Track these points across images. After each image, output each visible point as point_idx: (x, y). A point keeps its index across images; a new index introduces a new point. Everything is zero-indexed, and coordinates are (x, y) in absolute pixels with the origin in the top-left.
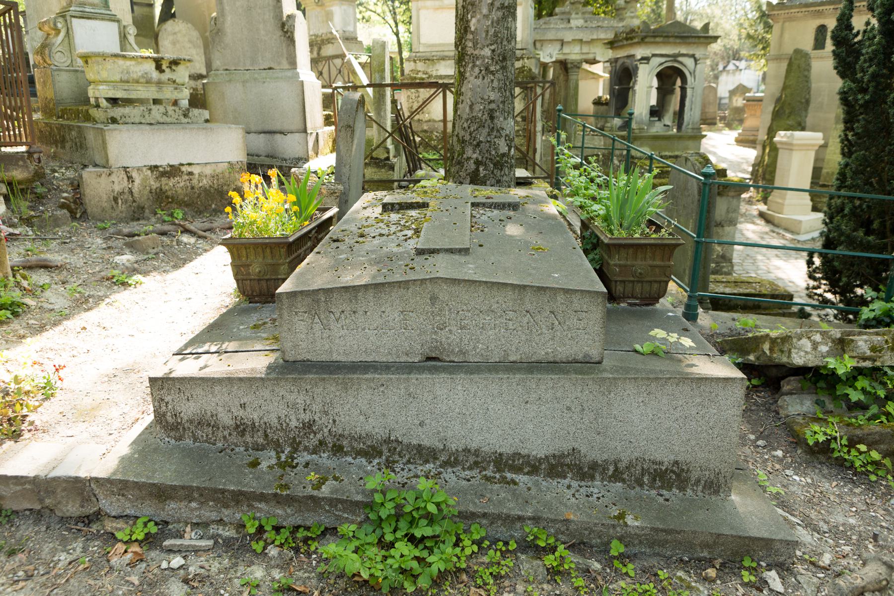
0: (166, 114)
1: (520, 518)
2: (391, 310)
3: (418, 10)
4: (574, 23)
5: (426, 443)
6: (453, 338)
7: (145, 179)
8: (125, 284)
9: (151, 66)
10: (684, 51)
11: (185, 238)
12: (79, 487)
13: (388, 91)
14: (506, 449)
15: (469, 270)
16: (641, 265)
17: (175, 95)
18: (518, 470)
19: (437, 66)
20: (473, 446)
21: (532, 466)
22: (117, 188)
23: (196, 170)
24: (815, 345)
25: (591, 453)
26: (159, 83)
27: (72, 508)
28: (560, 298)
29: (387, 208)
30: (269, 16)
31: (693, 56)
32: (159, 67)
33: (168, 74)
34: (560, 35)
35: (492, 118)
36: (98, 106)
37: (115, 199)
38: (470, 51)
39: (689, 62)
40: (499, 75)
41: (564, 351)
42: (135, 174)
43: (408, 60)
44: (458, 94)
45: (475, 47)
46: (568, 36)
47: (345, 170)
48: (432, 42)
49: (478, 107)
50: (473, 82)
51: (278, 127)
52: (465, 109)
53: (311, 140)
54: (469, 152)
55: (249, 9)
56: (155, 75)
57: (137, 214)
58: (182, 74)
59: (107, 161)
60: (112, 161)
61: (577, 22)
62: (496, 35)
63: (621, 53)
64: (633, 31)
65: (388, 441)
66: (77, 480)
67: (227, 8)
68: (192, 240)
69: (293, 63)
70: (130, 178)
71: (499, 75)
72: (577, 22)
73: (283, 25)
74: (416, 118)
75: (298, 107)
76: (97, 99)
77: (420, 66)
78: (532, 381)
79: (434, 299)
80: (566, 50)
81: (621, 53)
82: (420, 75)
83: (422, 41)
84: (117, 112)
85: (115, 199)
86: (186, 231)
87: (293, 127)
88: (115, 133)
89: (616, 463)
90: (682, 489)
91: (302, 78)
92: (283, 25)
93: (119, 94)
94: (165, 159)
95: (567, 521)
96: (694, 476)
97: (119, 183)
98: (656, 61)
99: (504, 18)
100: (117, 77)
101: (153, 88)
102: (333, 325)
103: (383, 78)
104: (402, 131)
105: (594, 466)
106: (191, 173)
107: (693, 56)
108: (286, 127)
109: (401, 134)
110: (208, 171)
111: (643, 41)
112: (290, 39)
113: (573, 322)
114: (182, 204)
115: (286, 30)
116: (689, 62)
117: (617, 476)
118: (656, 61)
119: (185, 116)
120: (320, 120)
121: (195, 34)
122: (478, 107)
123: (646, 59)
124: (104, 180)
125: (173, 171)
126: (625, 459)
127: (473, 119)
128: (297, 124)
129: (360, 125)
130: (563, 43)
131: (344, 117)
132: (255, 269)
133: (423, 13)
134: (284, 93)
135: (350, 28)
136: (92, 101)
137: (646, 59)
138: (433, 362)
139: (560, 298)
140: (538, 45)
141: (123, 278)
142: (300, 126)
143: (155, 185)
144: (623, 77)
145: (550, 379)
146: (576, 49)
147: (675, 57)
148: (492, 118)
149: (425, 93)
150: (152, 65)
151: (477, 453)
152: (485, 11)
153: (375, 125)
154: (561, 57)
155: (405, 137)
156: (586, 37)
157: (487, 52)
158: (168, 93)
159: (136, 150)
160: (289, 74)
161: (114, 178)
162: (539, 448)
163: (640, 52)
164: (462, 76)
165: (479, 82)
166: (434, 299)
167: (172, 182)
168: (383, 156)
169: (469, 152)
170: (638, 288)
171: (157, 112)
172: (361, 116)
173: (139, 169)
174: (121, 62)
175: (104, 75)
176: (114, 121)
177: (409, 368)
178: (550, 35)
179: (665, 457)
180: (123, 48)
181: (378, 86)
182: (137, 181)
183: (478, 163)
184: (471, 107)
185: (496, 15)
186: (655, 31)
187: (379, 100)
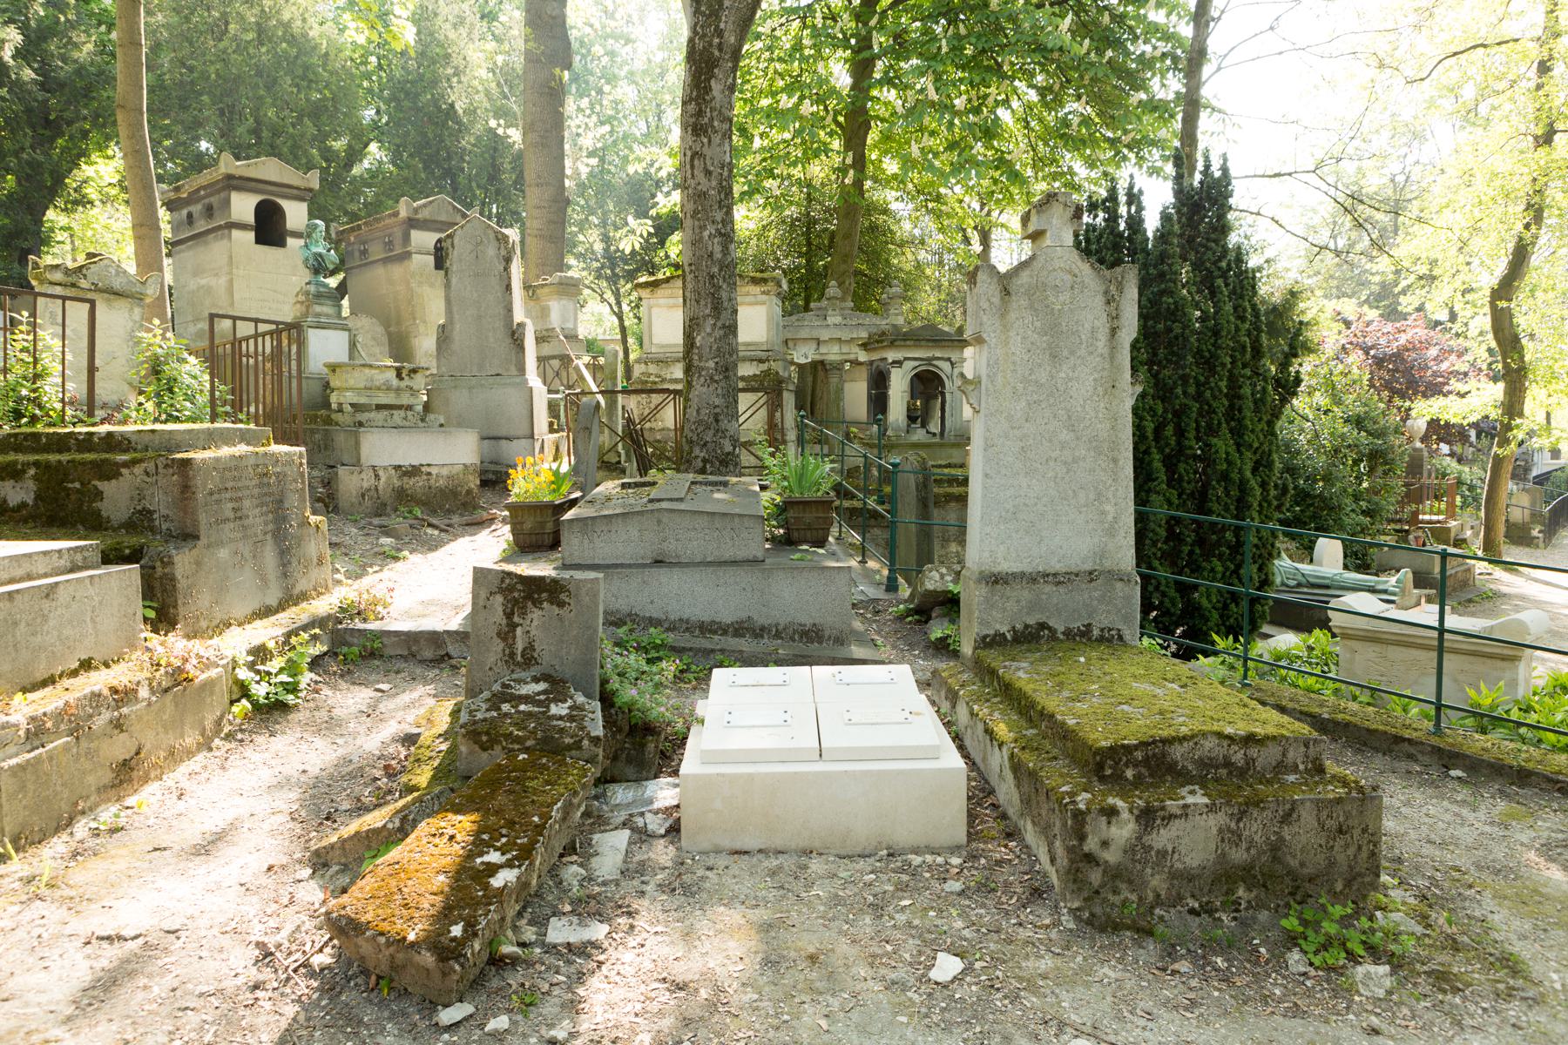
0: (405, 419)
1: (713, 651)
2: (632, 530)
3: (650, 308)
4: (830, 320)
5: (655, 615)
6: (671, 547)
7: (389, 478)
8: (396, 559)
9: (392, 374)
10: (938, 355)
11: (429, 531)
12: (435, 638)
13: (620, 397)
14: (706, 618)
15: (682, 506)
16: (809, 516)
17: (411, 401)
18: (715, 632)
19: (672, 369)
20: (685, 617)
21: (723, 630)
22: (365, 485)
23: (434, 471)
24: (942, 576)
25: (761, 620)
26: (398, 389)
27: (428, 654)
28: (737, 520)
29: (624, 486)
30: (499, 324)
31: (949, 359)
32: (399, 376)
33: (407, 382)
34: (815, 334)
35: (717, 421)
36: (340, 410)
37: (363, 495)
38: (696, 363)
39: (945, 366)
40: (722, 384)
41: (742, 554)
42: (381, 473)
43: (638, 361)
44: (687, 400)
45: (700, 359)
46: (825, 335)
47: (582, 467)
48: (665, 342)
49: (705, 411)
50: (699, 389)
51: (503, 433)
52: (692, 413)
53: (538, 446)
54: (697, 451)
55: (480, 317)
56: (395, 382)
57: (380, 510)
58: (419, 381)
59: (359, 460)
60: (363, 461)
61: (835, 319)
62: (718, 349)
63: (875, 356)
64: (883, 333)
65: (630, 615)
66: (435, 633)
67: (456, 316)
68: (436, 532)
69: (522, 370)
70: (377, 476)
71: (722, 384)
72: (835, 319)
73: (513, 333)
74: (648, 425)
75: (525, 412)
76: (340, 404)
77: (652, 368)
78: (720, 571)
79: (659, 522)
80: (823, 350)
81: (875, 356)
82: (652, 378)
83: (655, 341)
84: (363, 417)
85: (363, 495)
86: (430, 525)
87: (520, 433)
88: (369, 436)
89: (777, 625)
90: (820, 643)
91: (531, 384)
92: (513, 333)
93: (363, 400)
94: (409, 458)
95: (741, 652)
96: (827, 633)
97: (367, 480)
98: (909, 365)
99: (726, 335)
100: (362, 385)
101: (392, 395)
102: (596, 540)
103: (615, 385)
104: (634, 436)
105: (763, 629)
106: (429, 474)
107: (949, 359)
108: (512, 433)
109: (632, 439)
110: (445, 471)
111: (892, 345)
112: (519, 346)
113: (745, 535)
114: (420, 503)
115: (516, 337)
116: (945, 366)
117: (778, 635)
118: (909, 365)
119: (423, 420)
120: (545, 427)
121: (380, 330)
122: (705, 411)
123: (898, 363)
124: (355, 477)
125: (414, 471)
126: (782, 622)
127: (699, 422)
128: (525, 431)
129: (595, 428)
130: (819, 342)
131: (576, 417)
132: (528, 526)
133: (654, 311)
134: (512, 398)
135: (570, 325)
136: (334, 406)
137: (898, 363)
138: (658, 562)
139: (737, 520)
140: (791, 344)
141: (393, 553)
142: (528, 432)
143: (397, 483)
144: (879, 381)
145: (731, 570)
146: (836, 349)
147: (929, 360)
148: (717, 421)
149: (656, 399)
150: (394, 373)
151: (687, 622)
152: (708, 330)
153: (606, 431)
154: (818, 358)
155: (635, 442)
156: (845, 335)
157: (711, 364)
158: (405, 400)
159: (387, 450)
160: (518, 380)
161: (363, 475)
162: (727, 617)
163: (891, 356)
164: (689, 384)
165: (705, 389)
166: (659, 522)
167: (413, 480)
168: (614, 460)
169: (697, 451)
170: (809, 534)
171: (398, 415)
172: (596, 421)
173: (385, 468)
174: (367, 371)
175: (352, 382)
176: (361, 424)
177: (644, 566)
178: (804, 334)
179: (807, 621)
180: (351, 358)
181: (610, 393)
182: (383, 480)
183: (705, 461)
184: (698, 411)
185: (718, 333)
186: (905, 334)
187: (612, 405)
